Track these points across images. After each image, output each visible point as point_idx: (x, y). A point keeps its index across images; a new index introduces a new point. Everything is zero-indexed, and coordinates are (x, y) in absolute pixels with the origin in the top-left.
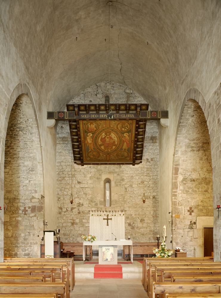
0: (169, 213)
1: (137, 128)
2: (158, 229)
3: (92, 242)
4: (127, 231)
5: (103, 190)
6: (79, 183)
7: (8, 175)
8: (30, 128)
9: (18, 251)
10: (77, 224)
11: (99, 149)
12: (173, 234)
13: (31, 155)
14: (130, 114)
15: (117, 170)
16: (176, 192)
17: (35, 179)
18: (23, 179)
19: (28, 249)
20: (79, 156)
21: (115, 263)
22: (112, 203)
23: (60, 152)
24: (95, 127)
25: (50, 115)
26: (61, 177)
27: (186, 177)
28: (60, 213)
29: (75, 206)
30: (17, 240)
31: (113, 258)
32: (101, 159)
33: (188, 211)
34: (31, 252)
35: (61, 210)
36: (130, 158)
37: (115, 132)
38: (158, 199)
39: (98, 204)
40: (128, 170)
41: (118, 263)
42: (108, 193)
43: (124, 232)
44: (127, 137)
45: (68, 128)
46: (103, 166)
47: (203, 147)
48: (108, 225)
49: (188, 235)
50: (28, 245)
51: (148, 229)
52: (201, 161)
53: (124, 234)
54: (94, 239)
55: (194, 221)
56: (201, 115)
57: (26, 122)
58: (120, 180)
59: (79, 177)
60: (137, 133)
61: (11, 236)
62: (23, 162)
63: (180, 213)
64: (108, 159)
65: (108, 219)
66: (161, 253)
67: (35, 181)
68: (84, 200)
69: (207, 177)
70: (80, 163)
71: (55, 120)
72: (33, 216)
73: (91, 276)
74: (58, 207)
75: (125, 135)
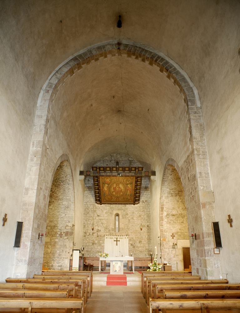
0: (158, 237)
1: (137, 181)
3: (106, 258)
4: (129, 249)
6: (98, 216)
8: (68, 181)
9: (54, 264)
11: (112, 194)
13: (68, 198)
14: (132, 173)
15: (123, 208)
17: (69, 213)
19: (61, 262)
21: (122, 273)
22: (120, 230)
23: (87, 196)
25: (81, 173)
26: (86, 212)
28: (85, 236)
29: (95, 232)
30: (54, 255)
33: (171, 236)
34: (63, 264)
35: (85, 234)
39: (111, 230)
40: (131, 208)
41: (124, 273)
43: (128, 250)
45: (93, 180)
48: (117, 245)
51: (144, 248)
53: (128, 252)
54: (107, 256)
55: (175, 243)
59: (98, 212)
61: (50, 252)
62: (62, 202)
64: (118, 200)
65: (117, 241)
69: (183, 213)
72: (66, 239)
73: (104, 284)
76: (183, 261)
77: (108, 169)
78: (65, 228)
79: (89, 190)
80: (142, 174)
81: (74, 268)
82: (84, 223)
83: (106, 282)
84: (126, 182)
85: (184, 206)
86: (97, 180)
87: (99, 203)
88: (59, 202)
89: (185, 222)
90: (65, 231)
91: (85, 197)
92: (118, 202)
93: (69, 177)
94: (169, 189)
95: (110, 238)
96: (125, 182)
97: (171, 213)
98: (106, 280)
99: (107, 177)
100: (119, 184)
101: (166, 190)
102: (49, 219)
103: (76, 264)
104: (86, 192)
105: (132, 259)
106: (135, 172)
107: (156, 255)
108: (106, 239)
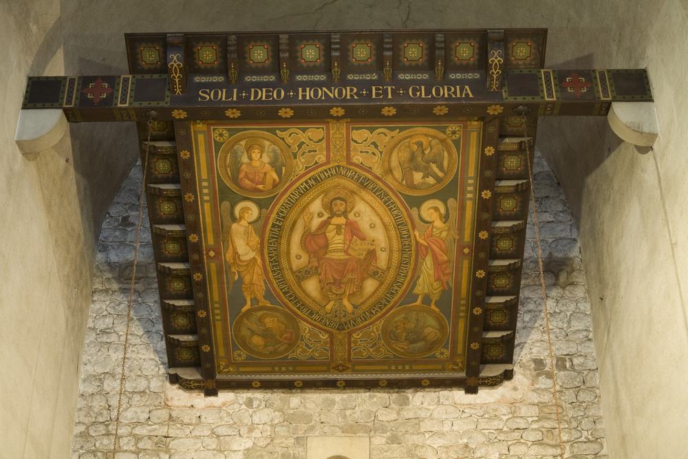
14: (455, 83)
15: (386, 416)
40: (443, 413)
64: (341, 353)
79: (124, 291)
80: (536, 92)
84: (407, 174)
92: (341, 368)
104: (101, 304)
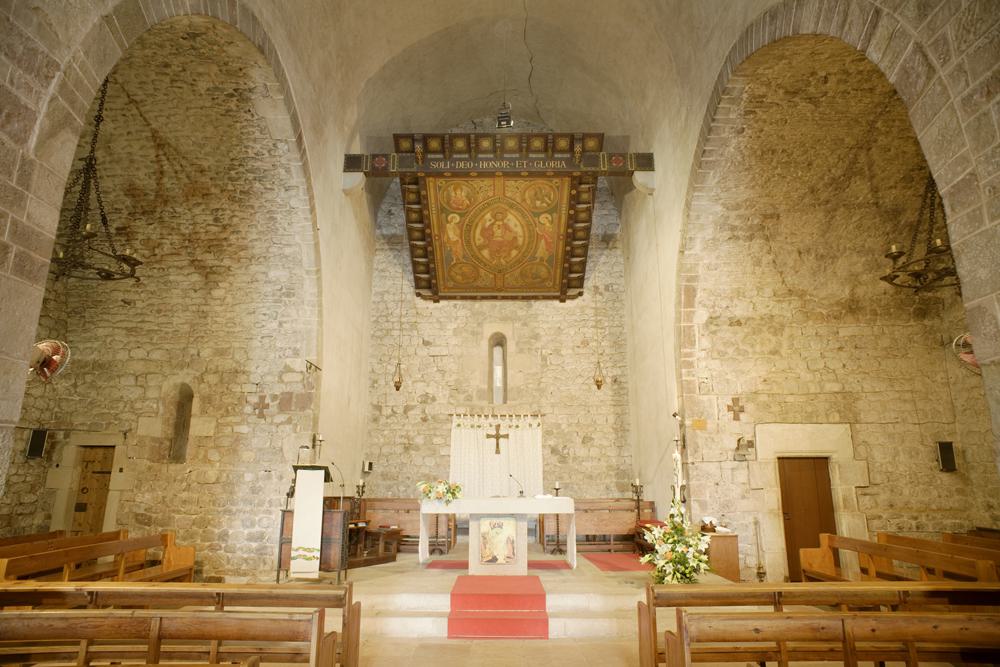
0: (674, 415)
1: (575, 200)
2: (628, 461)
3: (448, 502)
4: (547, 469)
5: (487, 361)
6: (426, 343)
7: (221, 305)
8: (282, 171)
9: (231, 527)
10: (417, 448)
11: (478, 259)
12: (691, 477)
13: (287, 251)
14: (557, 159)
15: (520, 313)
16: (690, 355)
17: (296, 317)
18: (264, 318)
19: (260, 520)
20: (426, 276)
21: (521, 569)
22: (509, 395)
23: (382, 271)
24: (467, 197)
25: (352, 163)
26: (381, 329)
27: (718, 314)
28: (375, 420)
29: (415, 403)
30: (231, 493)
31: (514, 554)
32: (481, 285)
33: (730, 408)
34: (270, 530)
35: (378, 413)
36: (555, 282)
37: (517, 209)
38: (625, 385)
39: (475, 398)
40: (549, 313)
41: (532, 565)
42: (498, 371)
43: (541, 469)
44: (548, 224)
45: (403, 214)
46: (487, 304)
47: (764, 227)
48: (498, 452)
49: (733, 480)
50: (262, 509)
51: (603, 464)
52: (757, 268)
53: (541, 476)
54: (453, 494)
55: (748, 437)
56: (765, 129)
57: (272, 152)
58: (531, 338)
59: (427, 330)
60: (572, 212)
61: (214, 480)
62: (263, 269)
63: (706, 413)
64: (499, 284)
65: (497, 437)
66: (674, 542)
67: (294, 325)
68: (438, 388)
69: (776, 312)
70: (430, 294)
71: (365, 173)
72: (282, 423)
73: (435, 629)
74: (371, 404)
75: (544, 219)
76: (781, 514)
77: (460, 144)
78: (280, 377)
79: (391, 249)
80: (597, 165)
81: (301, 552)
82: (373, 371)
83: (444, 622)
85: (783, 282)
86: (420, 212)
87: (430, 294)
88: (254, 268)
89: (784, 351)
90: (278, 390)
91: (375, 275)
92: (500, 290)
93: (286, 152)
94: (722, 204)
95: (472, 426)
96: (529, 202)
97: (729, 314)
98: (448, 609)
99: (457, 181)
100: (504, 214)
101: (711, 209)
102: (211, 344)
103: (308, 531)
104: (380, 257)
105: (564, 505)
106: (568, 156)
107: (678, 491)
108: (455, 432)
